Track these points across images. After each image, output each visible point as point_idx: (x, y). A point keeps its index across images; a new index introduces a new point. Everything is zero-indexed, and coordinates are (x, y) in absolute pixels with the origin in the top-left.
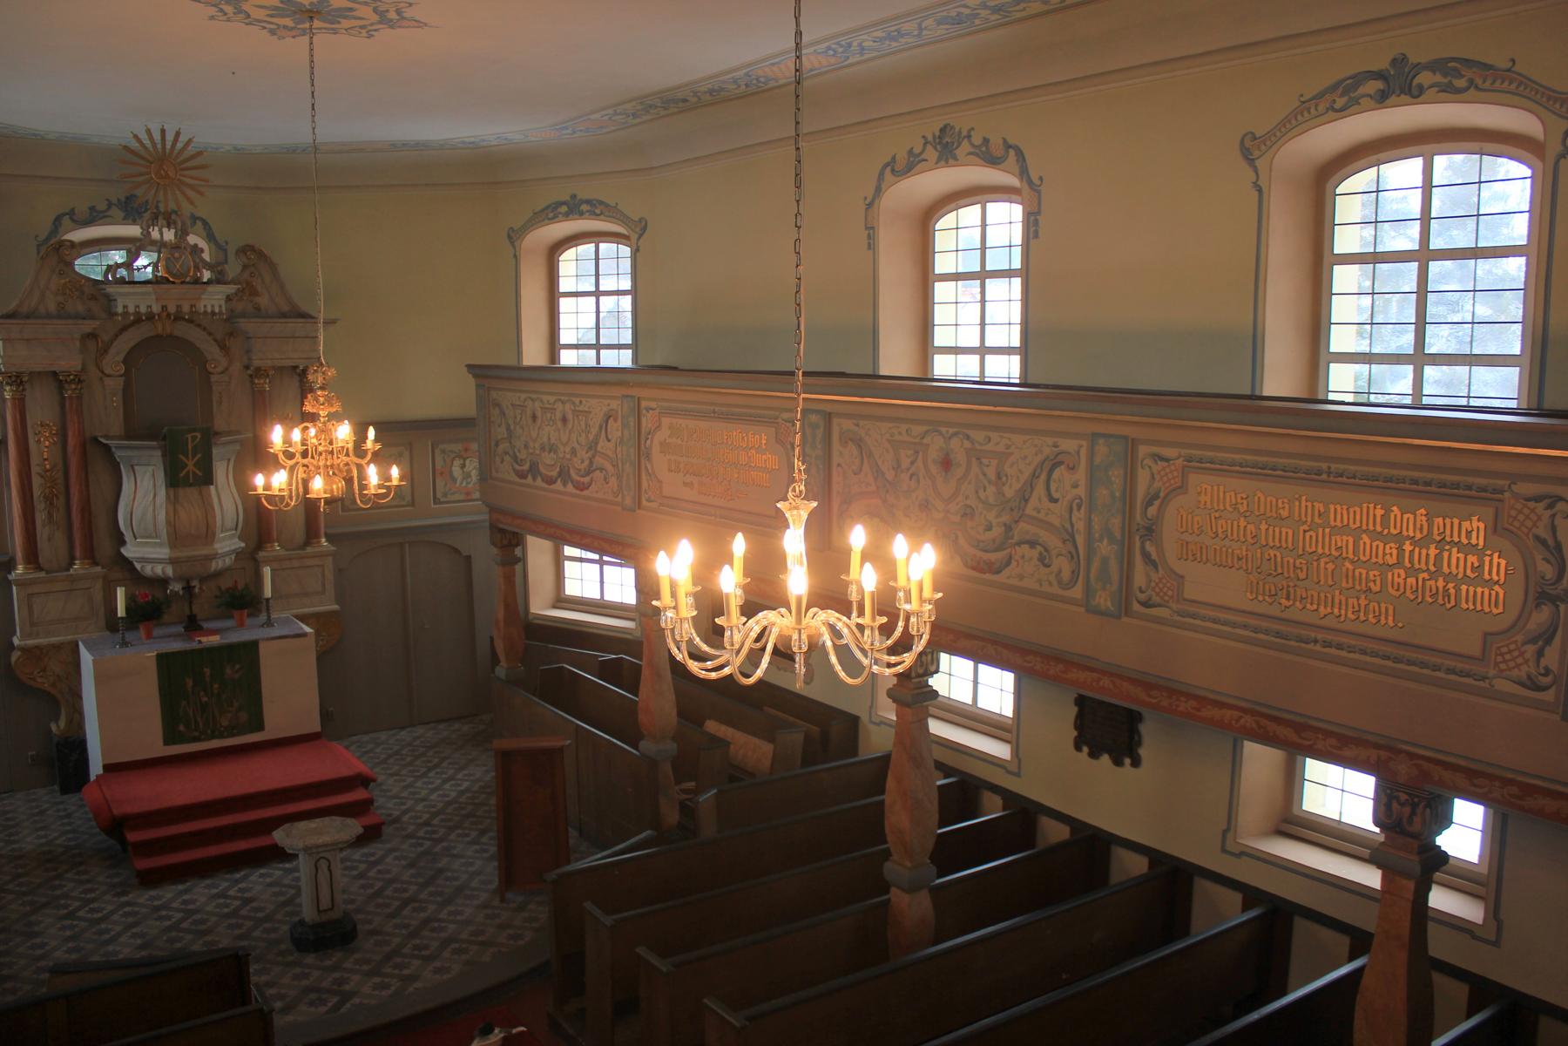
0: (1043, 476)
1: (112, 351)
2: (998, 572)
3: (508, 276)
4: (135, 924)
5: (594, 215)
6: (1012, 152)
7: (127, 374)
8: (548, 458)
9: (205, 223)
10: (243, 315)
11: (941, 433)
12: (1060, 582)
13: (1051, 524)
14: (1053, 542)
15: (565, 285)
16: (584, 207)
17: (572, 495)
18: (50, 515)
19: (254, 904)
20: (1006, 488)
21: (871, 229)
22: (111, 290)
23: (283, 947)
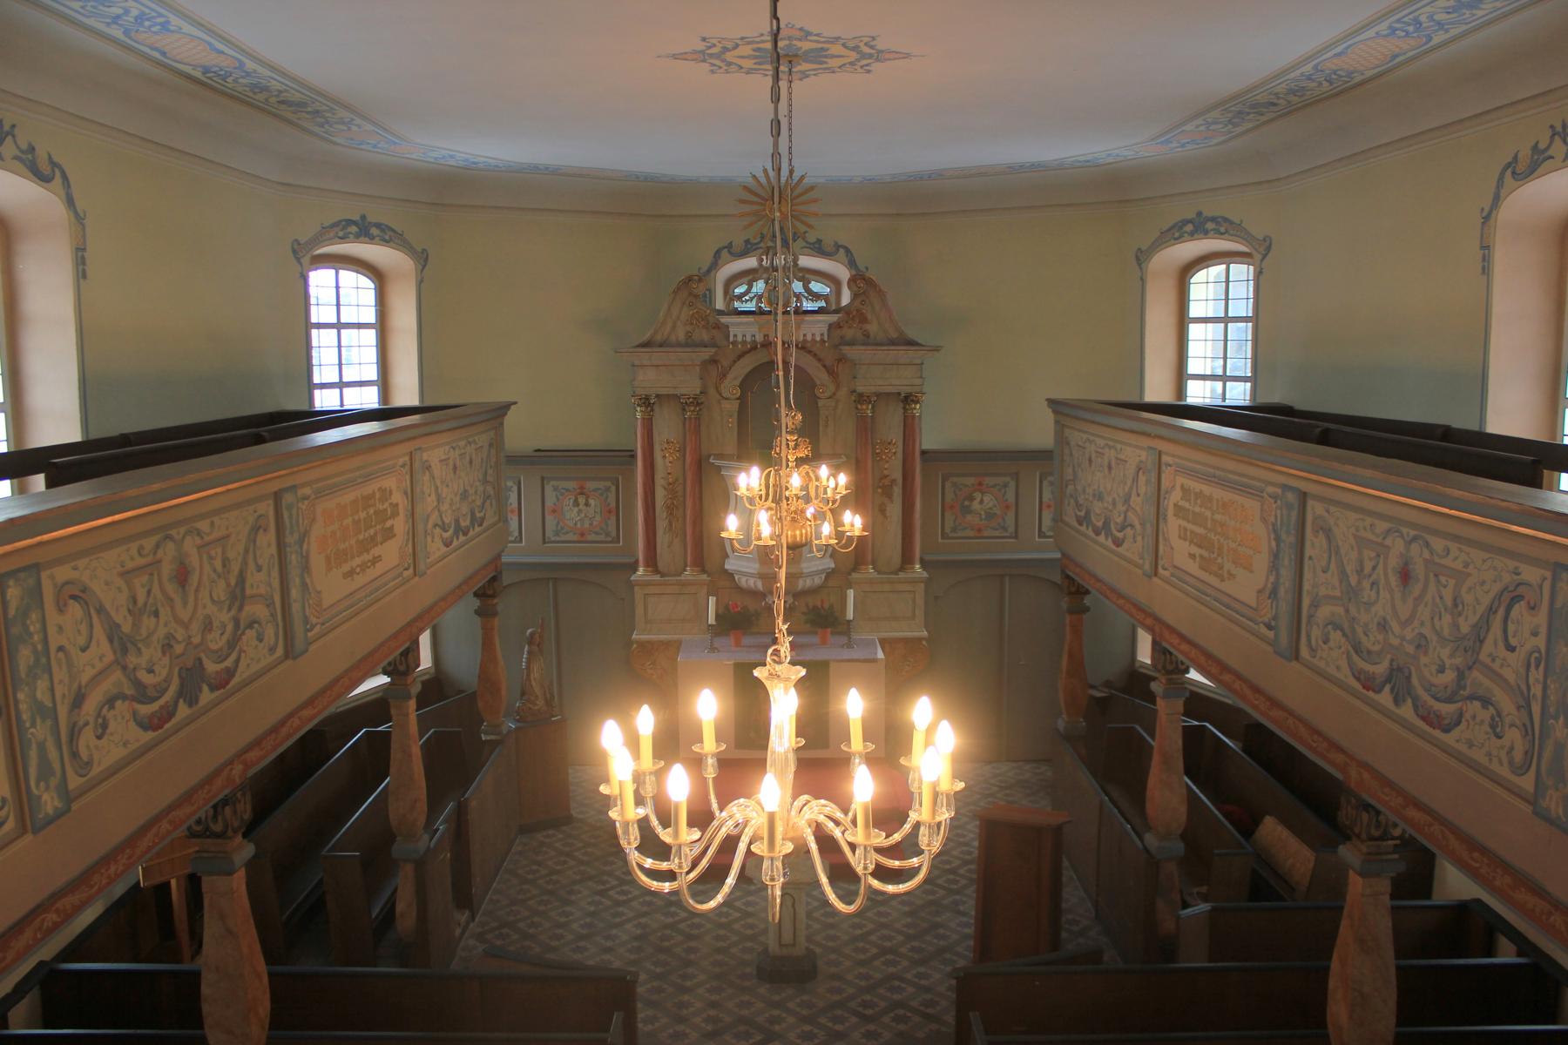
0: (1501, 612)
1: (730, 376)
2: (1447, 730)
3: (1130, 300)
4: (645, 914)
5: (1220, 234)
6: (58, 174)
7: (742, 399)
8: (1097, 507)
9: (848, 251)
10: (852, 343)
11: (1402, 536)
12: (1511, 763)
13: (1506, 681)
14: (1507, 705)
15: (1195, 310)
16: (1210, 226)
17: (1105, 548)
18: (670, 524)
19: (750, 920)
20: (1461, 620)
21: (1486, 248)
22: (724, 320)
23: (748, 970)
